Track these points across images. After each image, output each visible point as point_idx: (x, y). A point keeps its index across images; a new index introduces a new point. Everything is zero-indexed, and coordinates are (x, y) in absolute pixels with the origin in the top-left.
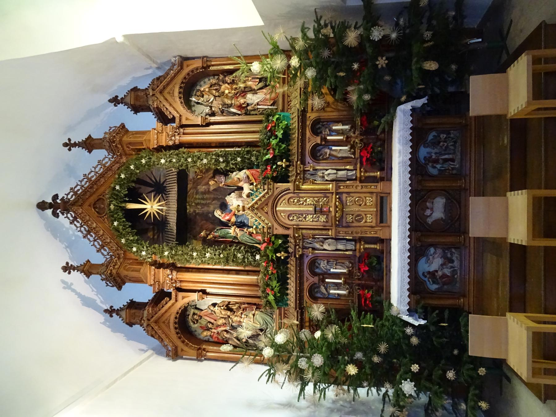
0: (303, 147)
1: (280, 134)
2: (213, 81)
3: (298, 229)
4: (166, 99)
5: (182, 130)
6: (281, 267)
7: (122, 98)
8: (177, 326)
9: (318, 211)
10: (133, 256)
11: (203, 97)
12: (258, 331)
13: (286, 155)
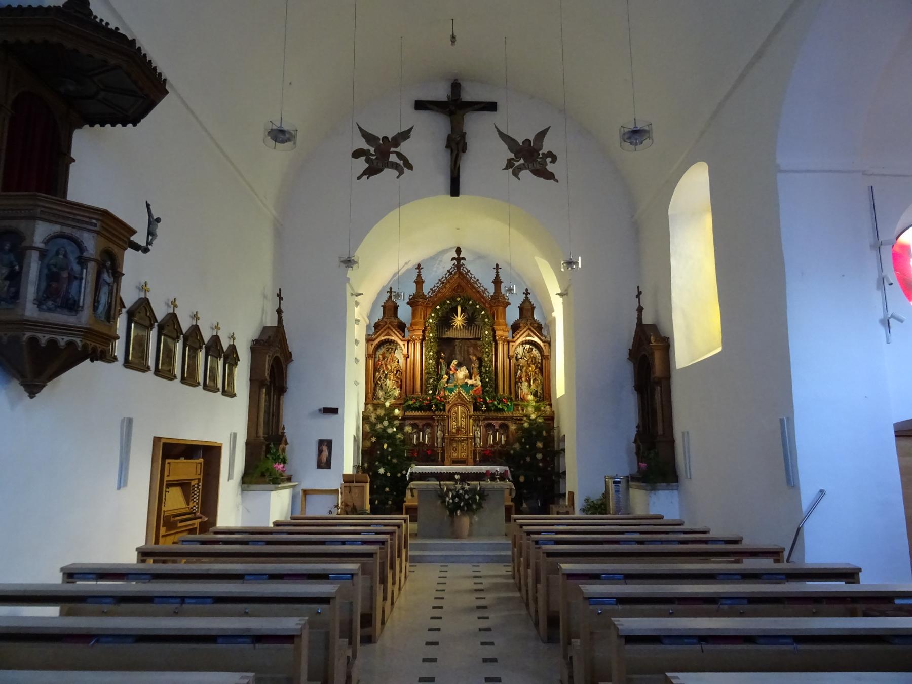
0: (493, 419)
1: (500, 406)
3: (449, 417)
6: (425, 405)
8: (104, 23)
9: (458, 429)
10: (428, 312)
13: (489, 410)
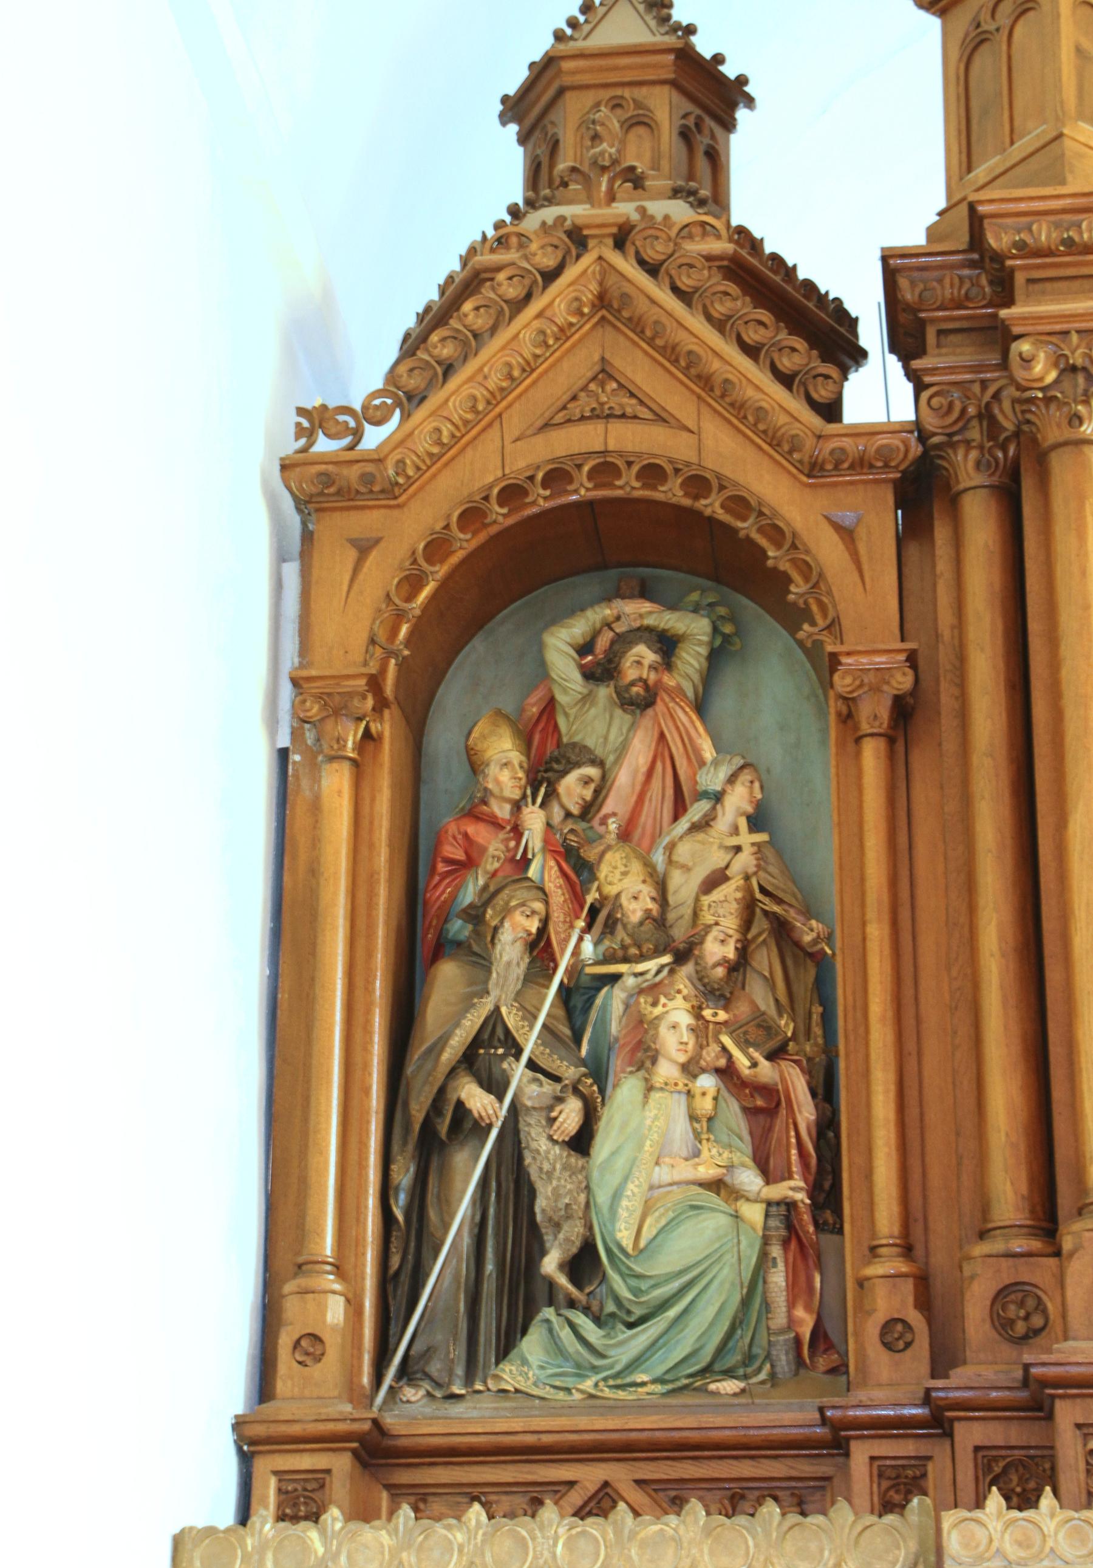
12: (573, 1231)
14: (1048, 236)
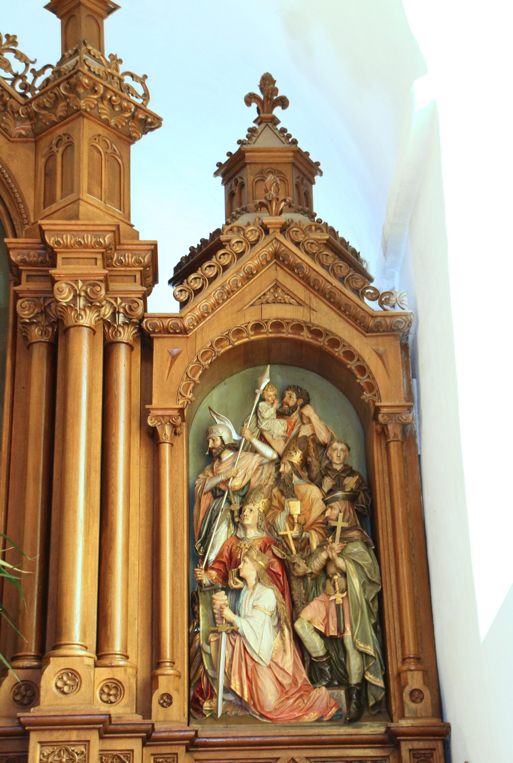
2: (337, 454)
4: (249, 276)
5: (126, 335)
7: (275, 121)
11: (280, 414)
14: (91, 240)
